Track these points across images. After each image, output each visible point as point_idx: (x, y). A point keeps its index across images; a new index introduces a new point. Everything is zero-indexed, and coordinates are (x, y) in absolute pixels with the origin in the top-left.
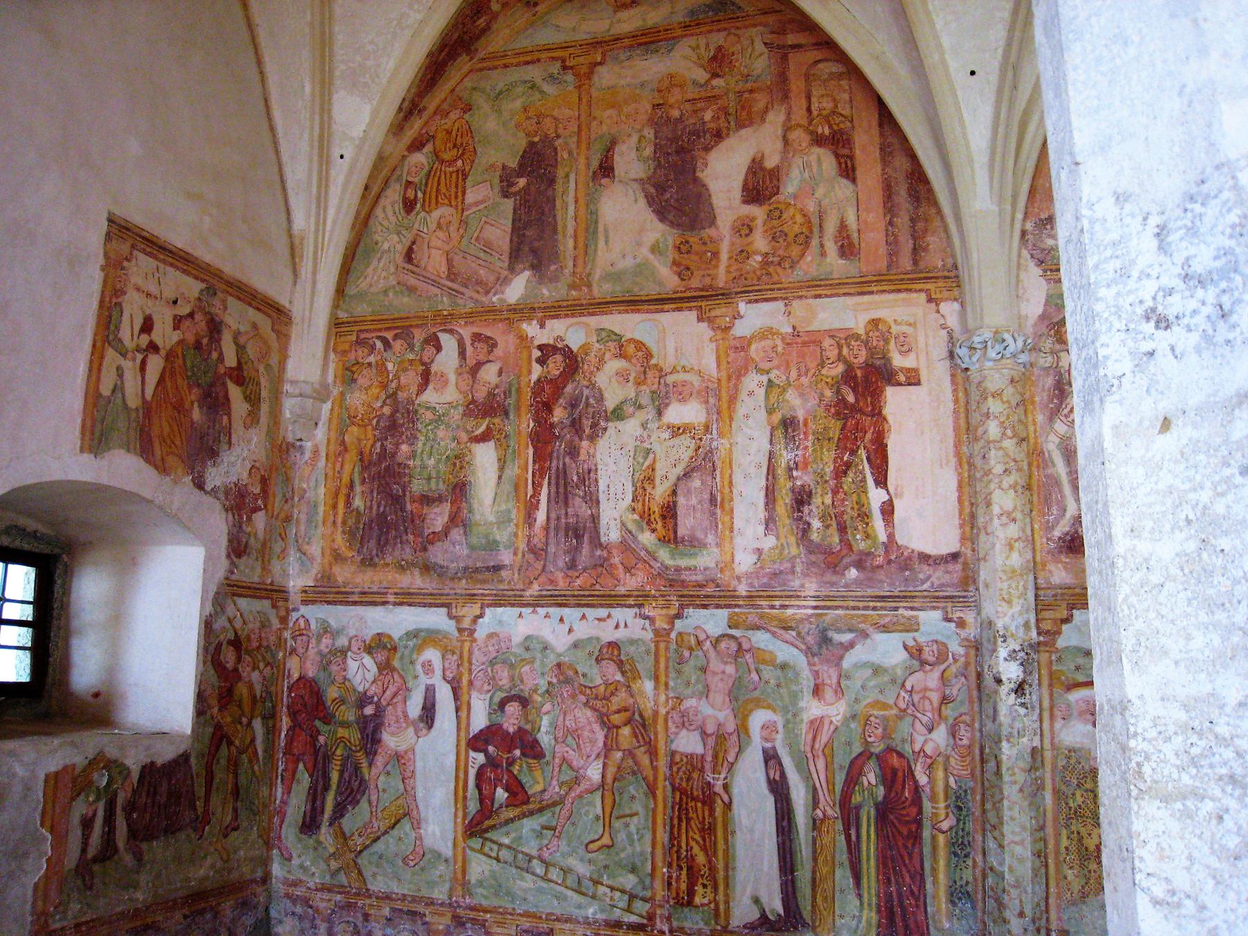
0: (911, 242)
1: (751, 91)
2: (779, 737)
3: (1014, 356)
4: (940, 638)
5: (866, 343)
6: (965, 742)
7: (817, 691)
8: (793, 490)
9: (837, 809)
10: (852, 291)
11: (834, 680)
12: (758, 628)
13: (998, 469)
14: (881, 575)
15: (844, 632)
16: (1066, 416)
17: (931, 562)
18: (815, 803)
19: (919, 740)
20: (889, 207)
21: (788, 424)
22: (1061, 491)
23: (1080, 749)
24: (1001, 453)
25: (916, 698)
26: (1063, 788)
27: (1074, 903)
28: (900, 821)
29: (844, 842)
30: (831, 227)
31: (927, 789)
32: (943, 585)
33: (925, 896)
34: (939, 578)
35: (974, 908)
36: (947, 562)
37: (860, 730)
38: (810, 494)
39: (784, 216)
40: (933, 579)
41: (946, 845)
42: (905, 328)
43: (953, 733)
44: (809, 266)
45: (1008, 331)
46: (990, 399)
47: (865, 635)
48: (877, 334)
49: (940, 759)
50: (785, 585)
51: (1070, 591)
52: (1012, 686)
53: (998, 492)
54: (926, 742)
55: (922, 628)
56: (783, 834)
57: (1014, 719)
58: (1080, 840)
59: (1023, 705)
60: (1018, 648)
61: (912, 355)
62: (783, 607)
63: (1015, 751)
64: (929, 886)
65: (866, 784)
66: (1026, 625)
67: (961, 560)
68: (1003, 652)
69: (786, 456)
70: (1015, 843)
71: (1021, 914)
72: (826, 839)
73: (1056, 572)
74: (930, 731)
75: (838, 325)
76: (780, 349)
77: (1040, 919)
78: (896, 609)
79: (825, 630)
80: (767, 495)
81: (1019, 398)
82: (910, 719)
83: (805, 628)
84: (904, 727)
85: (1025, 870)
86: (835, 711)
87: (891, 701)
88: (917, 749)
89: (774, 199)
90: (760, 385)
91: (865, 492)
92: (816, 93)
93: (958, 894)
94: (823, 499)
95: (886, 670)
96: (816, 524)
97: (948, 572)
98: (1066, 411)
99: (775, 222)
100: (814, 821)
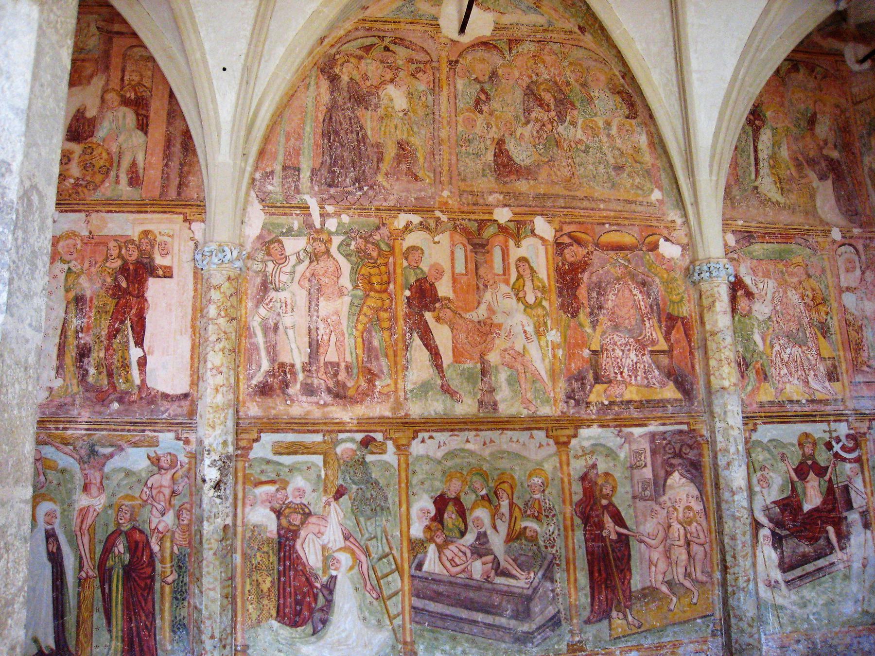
0: (178, 179)
1: (83, 61)
2: (57, 521)
3: (231, 262)
4: (173, 452)
5: (138, 247)
6: (186, 522)
7: (86, 488)
8: (78, 347)
9: (96, 571)
10: (134, 210)
11: (99, 480)
12: (46, 444)
13: (213, 338)
14: (135, 407)
15: (106, 447)
16: (267, 304)
17: (169, 399)
18: (81, 567)
19: (155, 522)
20: (167, 155)
21: (79, 301)
22: (258, 354)
23: (261, 526)
24: (216, 327)
25: (154, 492)
26: (249, 551)
27: (252, 627)
28: (139, 577)
29: (100, 595)
30: (126, 164)
31: (159, 555)
32: (176, 415)
33: (155, 628)
34: (174, 411)
35: (188, 634)
36: (180, 399)
37: (114, 515)
38: (90, 350)
39: (95, 153)
40: (171, 411)
41: (171, 593)
42: (166, 239)
43: (178, 516)
44: (107, 190)
45: (228, 245)
46: (212, 290)
47: (122, 449)
48: (147, 241)
49: (169, 534)
50: (67, 413)
51: (260, 421)
52: (212, 484)
53: (212, 353)
54: (159, 522)
55: (161, 445)
56: (57, 590)
57: (212, 506)
58: (258, 585)
59: (219, 497)
60: (217, 458)
61: (169, 257)
62: (65, 429)
63: (212, 528)
64: (158, 621)
65: (117, 552)
66: (225, 443)
67: (190, 398)
68: (207, 462)
69: (75, 323)
70: (210, 589)
71: (212, 637)
72: (87, 593)
73: (251, 408)
74: (163, 515)
75: (120, 233)
76: (79, 247)
77: (226, 639)
78: (144, 431)
79: (93, 445)
80: (59, 350)
81: (233, 291)
82: (150, 507)
83: (79, 444)
84: (145, 513)
85: (216, 608)
86: (97, 502)
87: (137, 495)
88: (153, 527)
89: (89, 140)
90: (62, 271)
91: (128, 349)
92: (129, 68)
93: (178, 625)
94: (98, 354)
95: (134, 473)
96: (92, 371)
97: (181, 407)
98: (267, 301)
99: (87, 157)
100: (80, 579)
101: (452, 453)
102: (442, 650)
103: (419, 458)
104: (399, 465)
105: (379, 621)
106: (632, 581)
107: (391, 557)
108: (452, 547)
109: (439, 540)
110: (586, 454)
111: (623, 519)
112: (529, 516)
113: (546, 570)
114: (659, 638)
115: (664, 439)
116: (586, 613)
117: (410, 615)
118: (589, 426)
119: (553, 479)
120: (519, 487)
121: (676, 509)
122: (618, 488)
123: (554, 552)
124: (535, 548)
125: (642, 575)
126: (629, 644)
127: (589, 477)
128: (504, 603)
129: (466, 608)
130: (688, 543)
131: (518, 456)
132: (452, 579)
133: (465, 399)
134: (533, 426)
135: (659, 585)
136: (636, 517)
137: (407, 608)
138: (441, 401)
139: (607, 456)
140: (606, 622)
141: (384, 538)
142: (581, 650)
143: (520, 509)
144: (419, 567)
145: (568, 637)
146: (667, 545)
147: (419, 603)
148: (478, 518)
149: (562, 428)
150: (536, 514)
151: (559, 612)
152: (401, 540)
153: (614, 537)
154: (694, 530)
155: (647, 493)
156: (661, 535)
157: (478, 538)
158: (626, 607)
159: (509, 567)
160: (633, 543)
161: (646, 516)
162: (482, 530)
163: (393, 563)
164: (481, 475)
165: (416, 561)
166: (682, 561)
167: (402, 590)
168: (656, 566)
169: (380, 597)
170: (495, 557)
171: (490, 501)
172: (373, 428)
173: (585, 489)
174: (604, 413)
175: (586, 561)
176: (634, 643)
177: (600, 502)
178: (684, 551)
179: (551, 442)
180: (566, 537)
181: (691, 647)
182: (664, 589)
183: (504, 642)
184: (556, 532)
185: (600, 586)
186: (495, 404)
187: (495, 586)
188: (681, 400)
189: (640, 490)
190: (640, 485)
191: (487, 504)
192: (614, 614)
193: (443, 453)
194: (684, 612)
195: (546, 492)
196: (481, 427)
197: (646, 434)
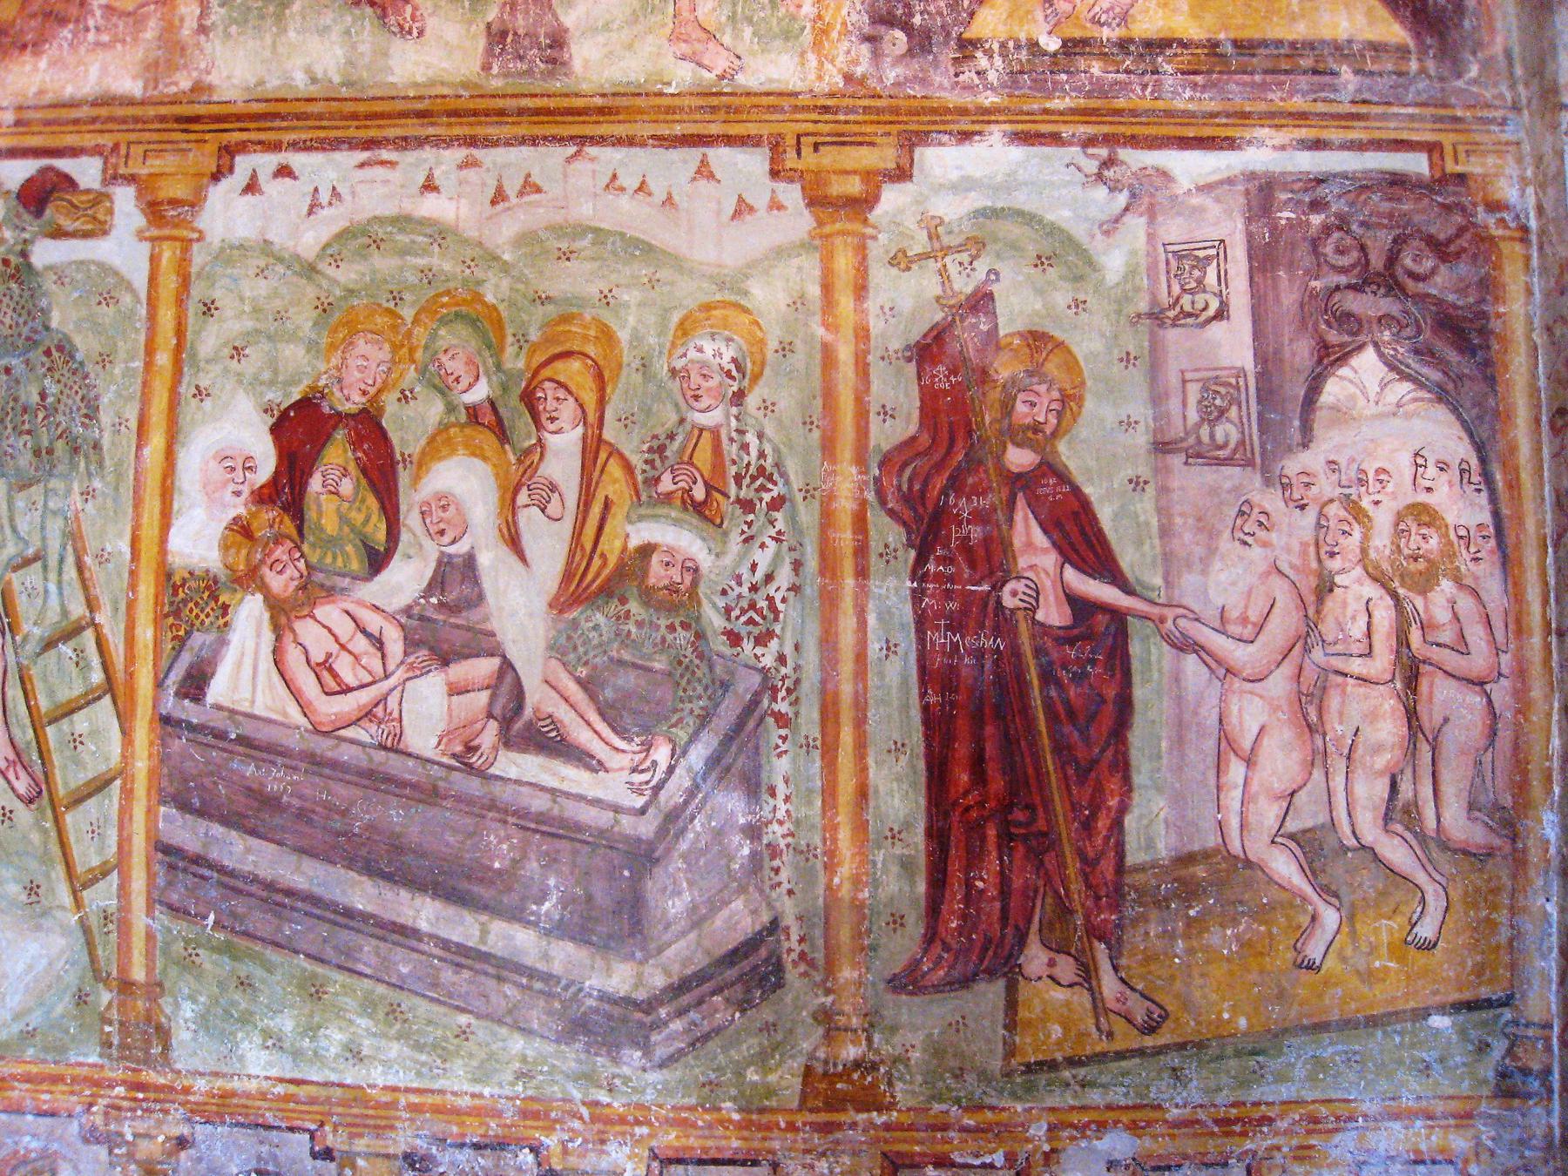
101: (364, 232)
102: (267, 1034)
103: (232, 253)
104: (153, 280)
105: (32, 889)
106: (1129, 821)
107: (89, 636)
108: (329, 613)
109: (280, 583)
110: (947, 250)
111: (1100, 534)
112: (668, 498)
113: (728, 740)
114: (1244, 1084)
115: (1317, 205)
116: (903, 946)
117: (151, 876)
118: (965, 137)
119: (786, 349)
120: (630, 377)
121: (1357, 512)
122: (1089, 404)
123: (768, 661)
124: (682, 636)
125: (1178, 800)
126: (1095, 1097)
127: (953, 347)
128: (533, 866)
129: (371, 870)
130: (1411, 673)
131: (643, 249)
132: (323, 746)
133: (431, 24)
134: (714, 129)
135: (1258, 849)
136: (1165, 532)
137: (139, 843)
138: (335, 36)
139: (1041, 261)
140: (991, 993)
141: (70, 560)
142: (870, 1101)
143: (628, 468)
144: (196, 684)
145: (809, 1041)
146: (1310, 674)
147: (187, 833)
148: (445, 501)
149: (841, 141)
150: (699, 493)
151: (774, 926)
152: (133, 574)
153: (1053, 614)
154: (1442, 615)
155: (1226, 431)
156: (1283, 624)
157: (438, 583)
158: (1095, 932)
159: (564, 713)
160: (1147, 652)
161: (1213, 535)
162: (462, 548)
163: (96, 661)
164: (473, 322)
165: (186, 659)
166: (1378, 749)
167: (123, 772)
168: (1250, 762)
169: (41, 793)
170: (507, 666)
171: (501, 432)
172: (70, 140)
173: (930, 403)
174: (1038, 85)
175: (916, 715)
176: (1118, 1096)
177: (999, 458)
178: (1387, 703)
179: (792, 194)
180: (829, 600)
181: (1393, 1138)
182: (1284, 867)
183: (527, 1032)
184: (784, 577)
185: (975, 830)
186: (558, 41)
187: (497, 789)
188: (1402, 52)
189: (1193, 416)
190: (1194, 391)
191: (488, 440)
192: (1035, 958)
193: (326, 233)
194: (1369, 976)
195: (752, 401)
196: (493, 131)
197: (1230, 181)
